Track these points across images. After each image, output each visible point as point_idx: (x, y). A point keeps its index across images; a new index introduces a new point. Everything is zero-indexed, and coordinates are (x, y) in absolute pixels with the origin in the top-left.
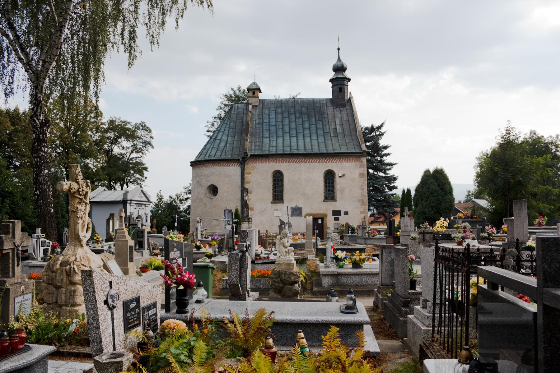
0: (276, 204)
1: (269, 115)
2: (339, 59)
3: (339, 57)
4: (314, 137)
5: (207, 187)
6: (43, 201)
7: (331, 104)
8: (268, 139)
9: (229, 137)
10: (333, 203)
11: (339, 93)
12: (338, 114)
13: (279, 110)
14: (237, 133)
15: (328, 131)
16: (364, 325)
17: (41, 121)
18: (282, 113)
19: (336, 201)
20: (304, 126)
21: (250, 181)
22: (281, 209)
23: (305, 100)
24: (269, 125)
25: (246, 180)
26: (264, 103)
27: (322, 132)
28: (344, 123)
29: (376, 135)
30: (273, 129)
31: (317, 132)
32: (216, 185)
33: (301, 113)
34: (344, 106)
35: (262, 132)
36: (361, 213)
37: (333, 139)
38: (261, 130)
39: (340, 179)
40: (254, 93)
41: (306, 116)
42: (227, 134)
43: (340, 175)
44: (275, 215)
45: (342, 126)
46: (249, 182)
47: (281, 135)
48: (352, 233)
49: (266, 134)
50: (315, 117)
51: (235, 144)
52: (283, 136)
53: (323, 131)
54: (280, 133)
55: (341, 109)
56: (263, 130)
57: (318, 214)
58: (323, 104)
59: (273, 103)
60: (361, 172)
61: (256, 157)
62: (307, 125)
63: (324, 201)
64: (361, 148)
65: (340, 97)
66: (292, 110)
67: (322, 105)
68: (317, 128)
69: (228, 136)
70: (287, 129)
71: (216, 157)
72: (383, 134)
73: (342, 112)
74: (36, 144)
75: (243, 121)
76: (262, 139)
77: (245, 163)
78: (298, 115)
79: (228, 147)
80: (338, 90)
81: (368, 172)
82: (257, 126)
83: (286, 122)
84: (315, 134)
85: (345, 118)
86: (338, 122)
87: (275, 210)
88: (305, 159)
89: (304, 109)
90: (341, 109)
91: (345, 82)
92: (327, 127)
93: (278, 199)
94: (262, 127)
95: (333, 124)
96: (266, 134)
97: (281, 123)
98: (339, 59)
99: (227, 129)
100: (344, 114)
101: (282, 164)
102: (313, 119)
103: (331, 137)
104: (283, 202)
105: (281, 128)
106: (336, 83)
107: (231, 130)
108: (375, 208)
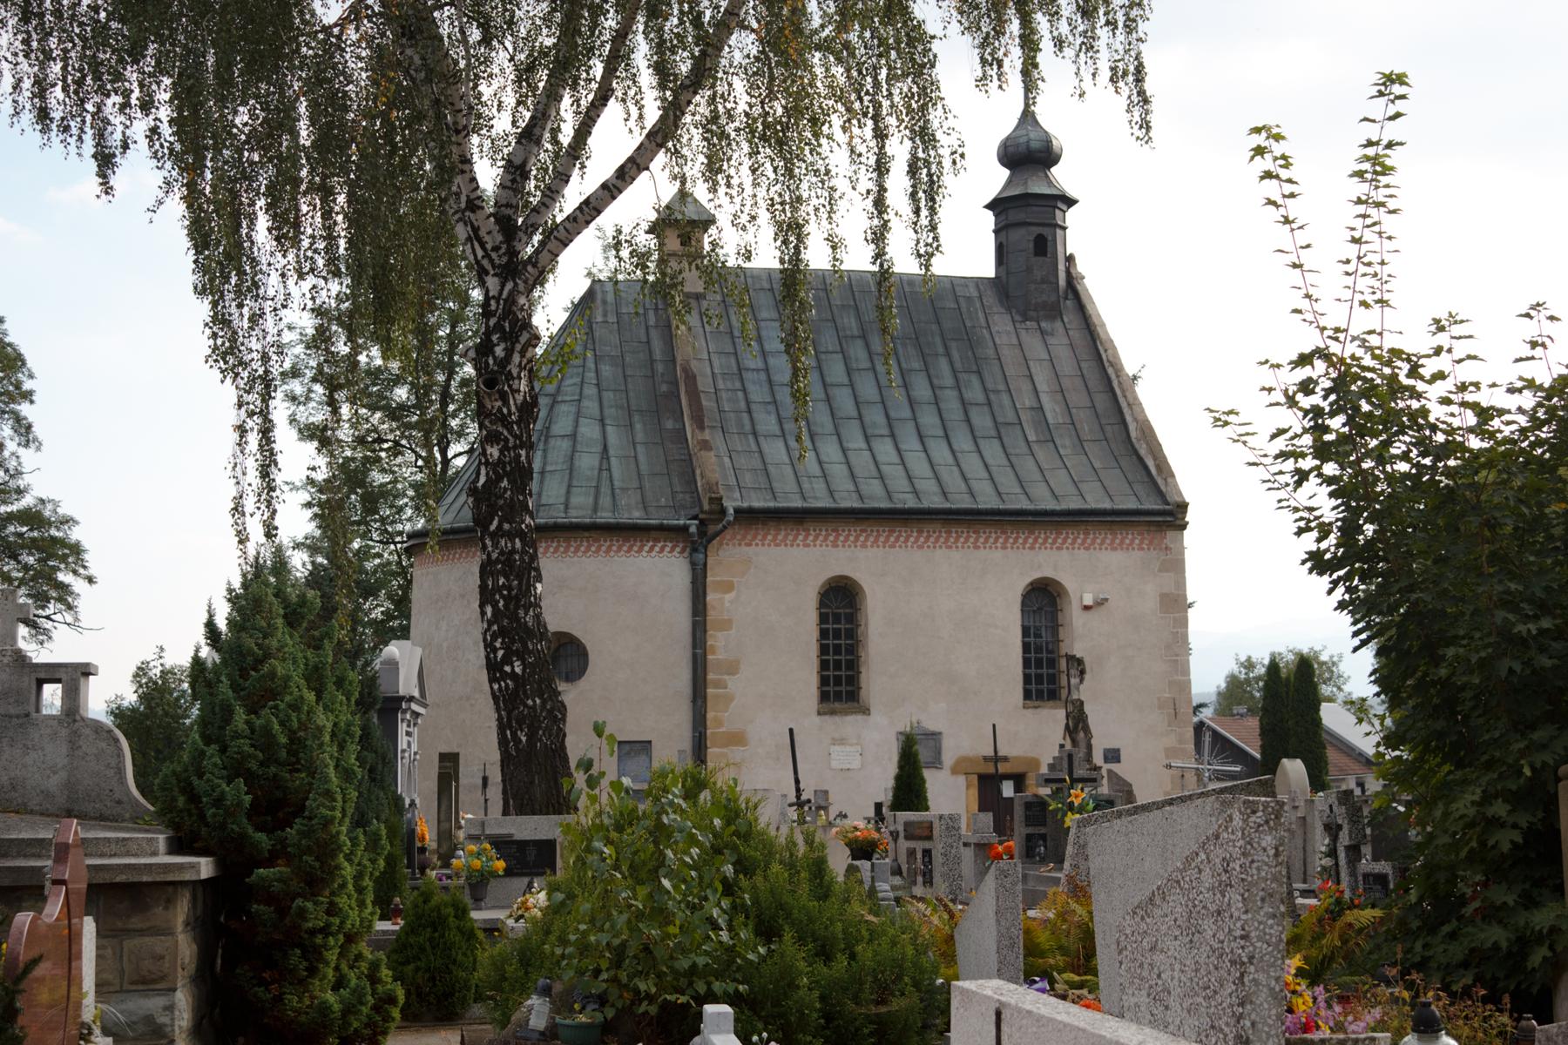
0: (837, 719)
2: (1028, 116)
4: (963, 442)
6: (544, 702)
9: (609, 429)
11: (1034, 259)
17: (520, 398)
21: (730, 621)
25: (712, 615)
27: (988, 422)
28: (1066, 383)
34: (1053, 311)
35: (749, 412)
38: (743, 405)
41: (912, 351)
42: (596, 412)
43: (1088, 600)
45: (1059, 397)
46: (726, 625)
47: (829, 428)
50: (948, 354)
51: (642, 458)
55: (1043, 324)
56: (748, 403)
58: (969, 299)
61: (754, 518)
62: (922, 390)
65: (1038, 274)
71: (573, 513)
73: (1051, 340)
74: (505, 483)
75: (652, 361)
77: (709, 541)
79: (616, 473)
80: (1031, 245)
85: (1067, 366)
87: (835, 742)
88: (949, 533)
90: (1043, 324)
92: (1005, 398)
93: (838, 697)
94: (744, 390)
95: (1026, 386)
98: (1028, 116)
99: (590, 391)
100: (1059, 343)
101: (861, 554)
102: (943, 364)
106: (1015, 215)
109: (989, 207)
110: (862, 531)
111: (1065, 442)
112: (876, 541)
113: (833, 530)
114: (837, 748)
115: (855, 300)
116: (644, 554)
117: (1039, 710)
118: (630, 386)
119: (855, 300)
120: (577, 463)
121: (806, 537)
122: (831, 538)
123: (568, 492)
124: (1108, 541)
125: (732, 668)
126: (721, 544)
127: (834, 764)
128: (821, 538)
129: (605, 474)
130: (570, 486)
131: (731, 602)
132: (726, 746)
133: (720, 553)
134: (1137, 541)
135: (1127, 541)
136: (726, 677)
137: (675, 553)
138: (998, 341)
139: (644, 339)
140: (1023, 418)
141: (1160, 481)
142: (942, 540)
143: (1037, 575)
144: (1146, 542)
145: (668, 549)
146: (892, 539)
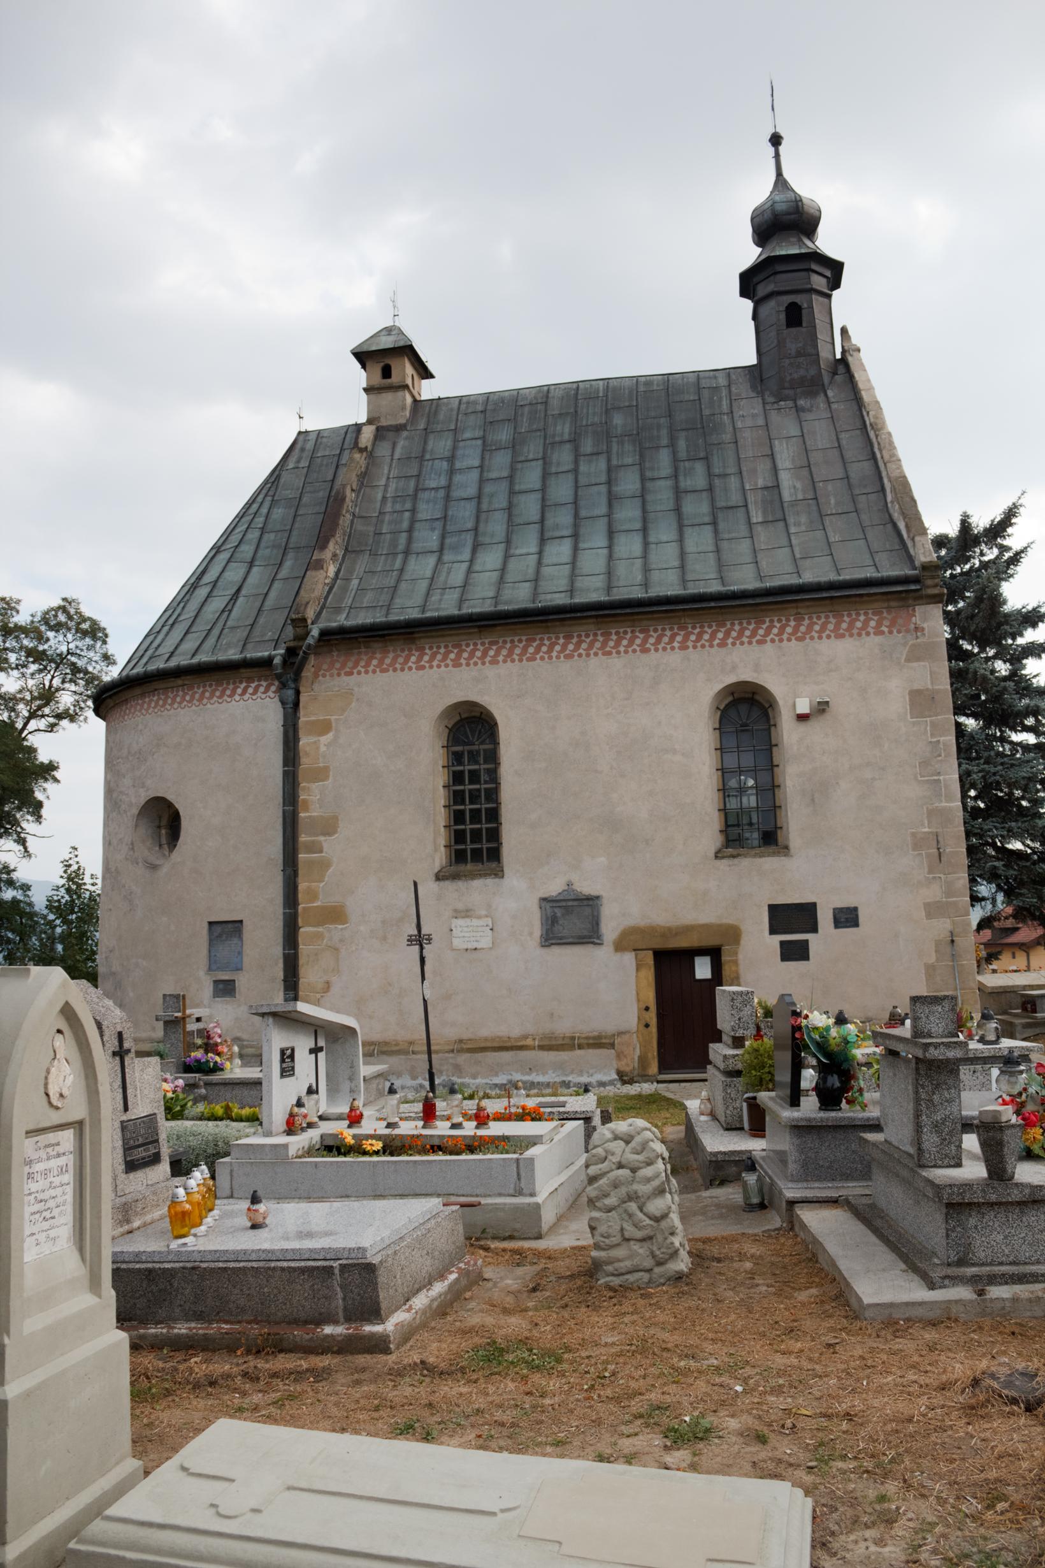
0: (460, 884)
1: (451, 459)
2: (780, 181)
3: (779, 173)
5: (135, 811)
7: (753, 387)
8: (432, 560)
9: (255, 570)
10: (770, 863)
11: (787, 332)
12: (785, 424)
13: (504, 435)
15: (735, 498)
19: (785, 850)
20: (614, 489)
21: (326, 769)
22: (489, 906)
23: (627, 383)
24: (448, 498)
25: (305, 762)
26: (436, 413)
27: (705, 508)
28: (815, 457)
29: (985, 565)
30: (464, 514)
31: (678, 510)
32: (170, 797)
33: (605, 434)
34: (813, 386)
35: (410, 530)
36: (933, 910)
37: (763, 536)
38: (405, 525)
39: (803, 727)
40: (387, 372)
41: (628, 447)
43: (803, 707)
45: (805, 472)
46: (321, 774)
48: (829, 1098)
49: (428, 538)
50: (672, 445)
51: (273, 594)
52: (508, 542)
53: (713, 500)
54: (496, 526)
55: (801, 402)
56: (413, 521)
57: (688, 929)
58: (716, 389)
59: (480, 408)
60: (916, 687)
62: (629, 483)
63: (718, 855)
64: (910, 559)
65: (792, 347)
66: (564, 429)
67: (706, 394)
68: (679, 493)
69: (251, 564)
70: (529, 507)
72: (1016, 559)
76: (405, 562)
78: (587, 446)
80: (783, 316)
81: (959, 728)
82: (388, 508)
83: (531, 477)
84: (672, 519)
86: (786, 456)
87: (458, 914)
88: (607, 635)
89: (618, 420)
90: (801, 402)
92: (734, 482)
93: (477, 856)
94: (413, 511)
95: (764, 466)
96: (428, 538)
97: (504, 486)
98: (780, 181)
99: (253, 535)
101: (490, 671)
102: (664, 457)
103: (750, 524)
104: (499, 873)
105: (505, 504)
107: (269, 537)
108: (999, 888)
110: (492, 643)
111: (799, 522)
113: (454, 646)
114: (460, 922)
115: (576, 406)
116: (237, 697)
117: (736, 861)
118: (297, 525)
119: (576, 406)
121: (420, 659)
122: (452, 656)
124: (831, 627)
125: (329, 827)
126: (316, 675)
127: (457, 943)
128: (439, 657)
129: (226, 613)
131: (328, 745)
132: (318, 924)
133: (316, 687)
134: (873, 624)
135: (859, 624)
136: (322, 838)
137: (270, 694)
138: (739, 425)
139: (330, 477)
140: (751, 498)
141: (909, 544)
142: (598, 645)
144: (887, 623)
145: (262, 689)
146: (531, 650)
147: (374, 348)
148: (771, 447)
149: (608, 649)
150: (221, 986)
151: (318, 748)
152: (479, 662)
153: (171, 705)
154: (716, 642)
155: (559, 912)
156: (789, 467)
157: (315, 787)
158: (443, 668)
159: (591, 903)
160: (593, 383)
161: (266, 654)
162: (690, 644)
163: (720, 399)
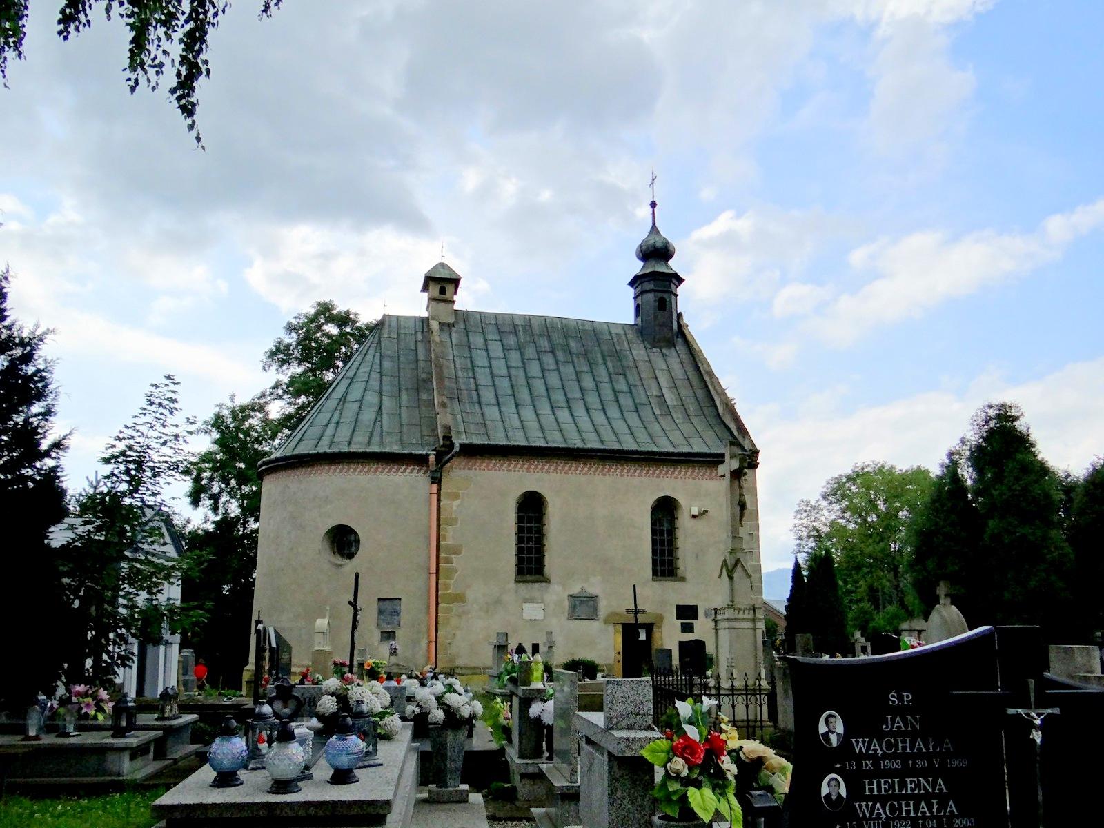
3: (654, 224)
14: (407, 389)
15: (644, 400)
16: (208, 764)
18: (520, 348)
21: (456, 520)
28: (678, 383)
33: (568, 350)
40: (442, 291)
41: (582, 361)
43: (695, 511)
44: (526, 616)
45: (675, 390)
49: (488, 395)
59: (493, 322)
61: (472, 452)
62: (588, 382)
67: (614, 336)
75: (417, 361)
83: (534, 369)
87: (526, 601)
89: (572, 343)
91: (672, 285)
92: (641, 390)
95: (654, 384)
99: (375, 376)
109: (632, 284)
111: (678, 416)
112: (555, 469)
120: (360, 417)
123: (352, 434)
129: (378, 424)
130: (354, 431)
131: (458, 506)
133: (451, 474)
136: (453, 556)
137: (421, 474)
142: (599, 470)
143: (663, 494)
146: (566, 468)
147: (438, 276)
148: (655, 374)
149: (604, 473)
150: (385, 635)
151: (452, 508)
152: (540, 471)
153: (353, 472)
154: (655, 475)
155: (577, 603)
156: (554, 368)
157: (450, 528)
158: (521, 472)
159: (593, 598)
160: (554, 319)
161: (424, 452)
162: (643, 475)
163: (623, 341)
